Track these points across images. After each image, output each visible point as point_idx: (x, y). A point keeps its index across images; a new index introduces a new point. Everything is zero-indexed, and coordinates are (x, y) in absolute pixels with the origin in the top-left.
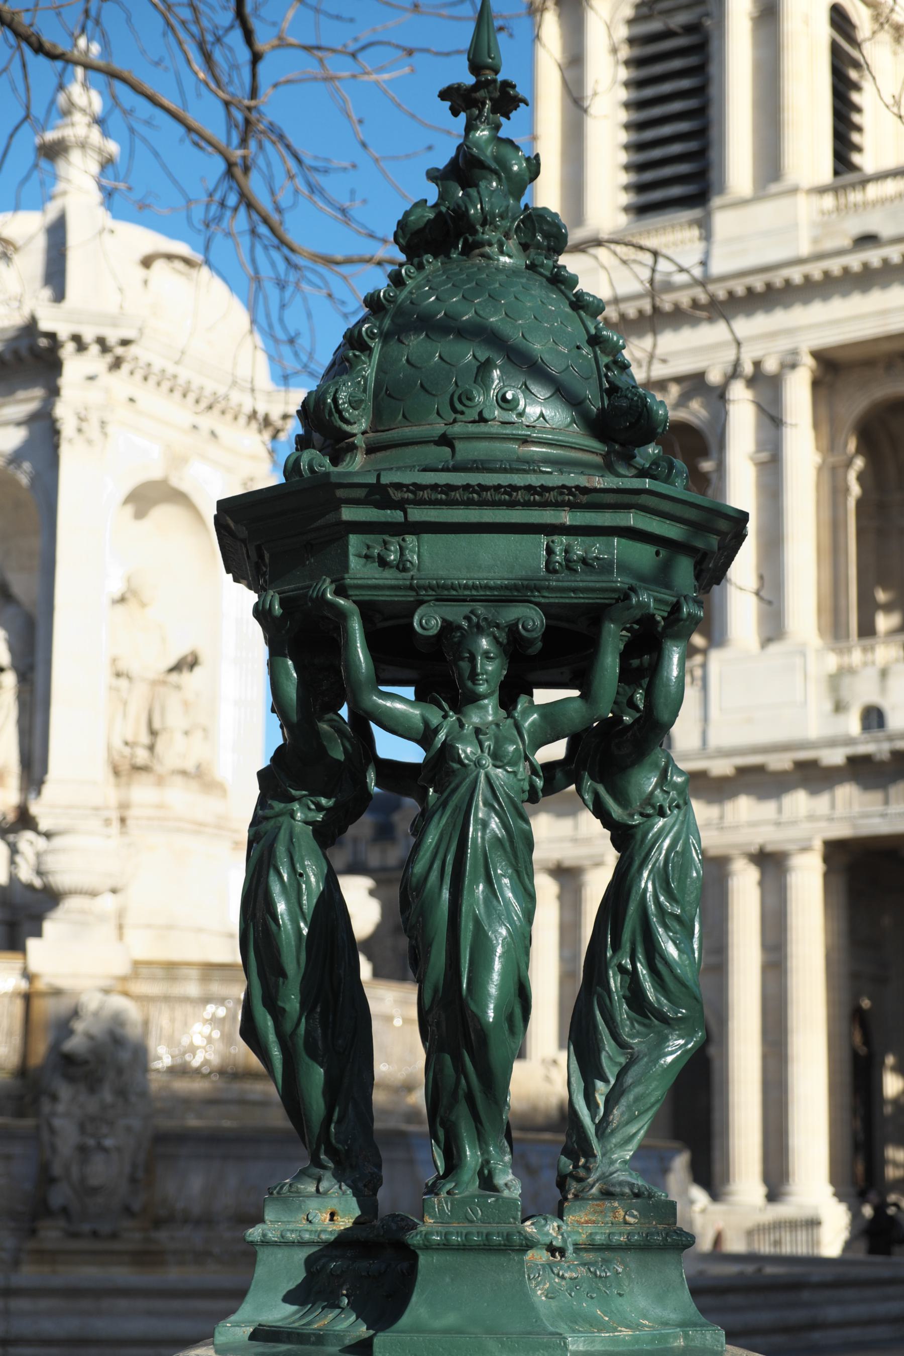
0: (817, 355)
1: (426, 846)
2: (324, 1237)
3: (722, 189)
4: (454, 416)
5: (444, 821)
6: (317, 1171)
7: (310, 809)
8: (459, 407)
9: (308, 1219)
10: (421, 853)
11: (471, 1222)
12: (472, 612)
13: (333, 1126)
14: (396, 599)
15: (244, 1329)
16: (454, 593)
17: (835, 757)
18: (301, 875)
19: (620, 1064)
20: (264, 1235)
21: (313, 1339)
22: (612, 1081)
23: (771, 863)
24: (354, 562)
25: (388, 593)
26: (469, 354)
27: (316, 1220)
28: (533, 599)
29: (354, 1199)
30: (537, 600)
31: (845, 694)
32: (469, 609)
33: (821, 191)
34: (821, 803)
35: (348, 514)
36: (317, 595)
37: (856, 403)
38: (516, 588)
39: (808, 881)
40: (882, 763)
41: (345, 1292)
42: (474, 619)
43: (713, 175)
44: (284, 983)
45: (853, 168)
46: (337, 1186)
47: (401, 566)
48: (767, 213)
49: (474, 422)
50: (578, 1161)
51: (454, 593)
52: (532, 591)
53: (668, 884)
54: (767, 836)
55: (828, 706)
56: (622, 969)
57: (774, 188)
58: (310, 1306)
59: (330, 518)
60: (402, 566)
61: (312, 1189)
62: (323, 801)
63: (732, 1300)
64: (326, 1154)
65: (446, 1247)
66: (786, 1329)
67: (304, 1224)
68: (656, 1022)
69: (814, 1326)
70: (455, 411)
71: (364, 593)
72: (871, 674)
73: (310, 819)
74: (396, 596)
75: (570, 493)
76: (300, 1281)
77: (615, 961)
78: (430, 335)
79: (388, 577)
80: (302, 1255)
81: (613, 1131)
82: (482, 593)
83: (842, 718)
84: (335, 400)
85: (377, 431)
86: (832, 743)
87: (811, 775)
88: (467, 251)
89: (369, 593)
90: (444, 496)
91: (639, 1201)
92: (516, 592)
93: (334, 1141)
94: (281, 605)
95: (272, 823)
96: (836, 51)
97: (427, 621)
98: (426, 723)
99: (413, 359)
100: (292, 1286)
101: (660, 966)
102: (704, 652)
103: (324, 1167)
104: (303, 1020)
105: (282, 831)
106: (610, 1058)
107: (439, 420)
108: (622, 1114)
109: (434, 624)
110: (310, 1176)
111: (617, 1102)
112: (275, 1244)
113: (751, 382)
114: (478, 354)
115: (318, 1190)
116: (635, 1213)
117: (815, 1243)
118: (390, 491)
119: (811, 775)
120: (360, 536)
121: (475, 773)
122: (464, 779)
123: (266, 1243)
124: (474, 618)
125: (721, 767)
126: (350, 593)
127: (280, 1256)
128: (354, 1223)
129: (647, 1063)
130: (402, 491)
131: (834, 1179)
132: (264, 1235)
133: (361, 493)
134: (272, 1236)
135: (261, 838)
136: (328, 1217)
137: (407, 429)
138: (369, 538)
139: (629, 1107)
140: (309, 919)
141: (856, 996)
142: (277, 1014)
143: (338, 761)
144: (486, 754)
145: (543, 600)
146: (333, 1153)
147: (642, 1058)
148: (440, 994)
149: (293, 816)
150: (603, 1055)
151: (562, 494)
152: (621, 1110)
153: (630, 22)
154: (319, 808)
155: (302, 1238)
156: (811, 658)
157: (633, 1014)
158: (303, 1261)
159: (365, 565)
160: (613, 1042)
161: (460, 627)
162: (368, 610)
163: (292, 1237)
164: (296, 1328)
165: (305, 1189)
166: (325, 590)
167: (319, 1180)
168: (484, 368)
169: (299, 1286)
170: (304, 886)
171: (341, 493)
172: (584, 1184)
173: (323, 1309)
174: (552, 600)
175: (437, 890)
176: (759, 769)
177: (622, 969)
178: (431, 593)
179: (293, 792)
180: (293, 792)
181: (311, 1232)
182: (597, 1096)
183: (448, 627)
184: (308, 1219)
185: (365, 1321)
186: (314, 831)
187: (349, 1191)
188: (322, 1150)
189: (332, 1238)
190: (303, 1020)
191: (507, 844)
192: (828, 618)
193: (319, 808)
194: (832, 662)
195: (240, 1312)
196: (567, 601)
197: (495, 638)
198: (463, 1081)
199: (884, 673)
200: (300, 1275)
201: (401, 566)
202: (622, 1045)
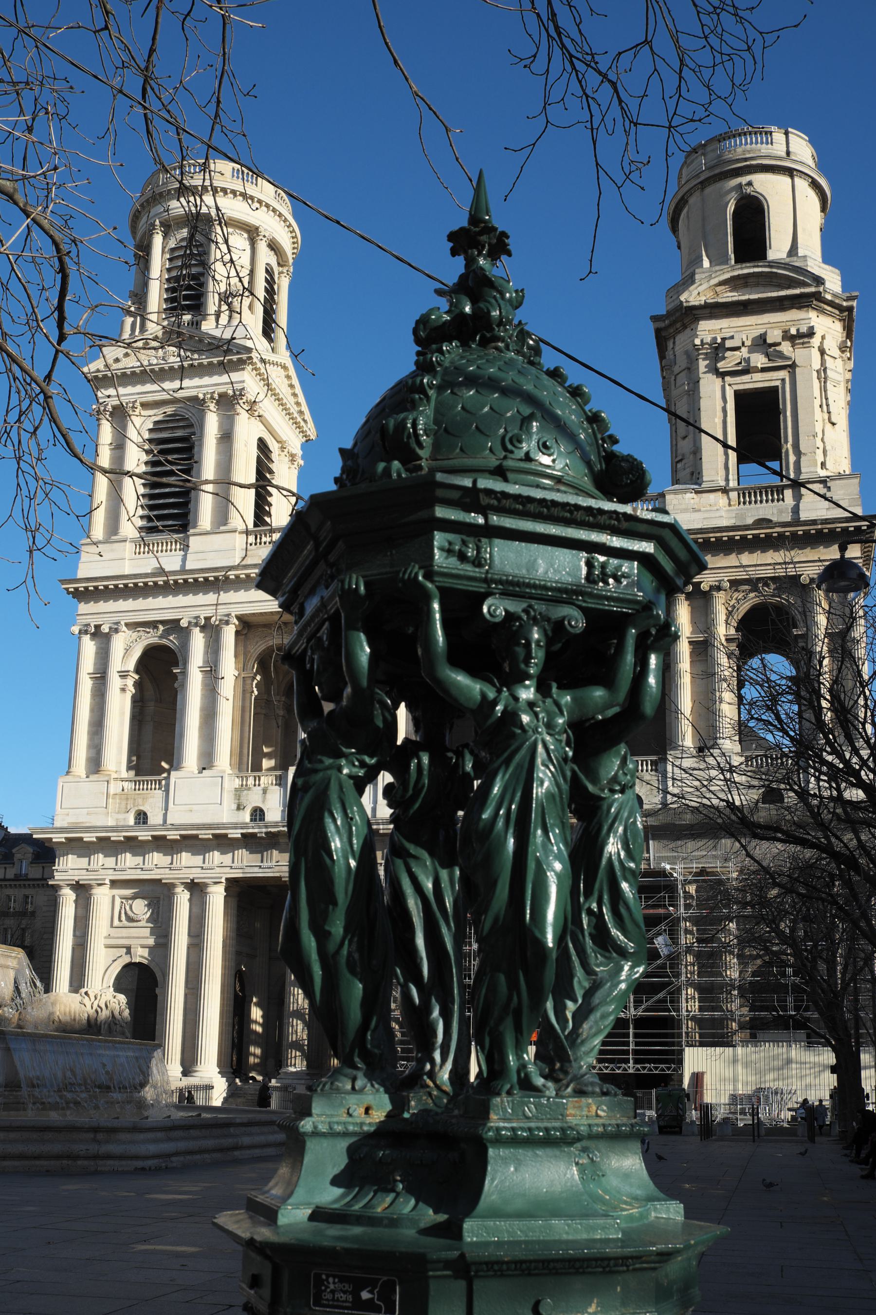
0: (238, 618)
1: (491, 798)
2: (366, 1128)
3: (195, 526)
4: (504, 453)
5: (507, 776)
6: (349, 1071)
7: (354, 765)
8: (510, 447)
9: (348, 1113)
10: (489, 802)
11: (528, 1118)
12: (530, 606)
13: (369, 1033)
14: (471, 589)
15: (304, 1211)
16: (517, 589)
17: (236, 834)
18: (352, 819)
19: (585, 988)
20: (315, 1127)
21: (385, 1222)
22: (580, 1001)
23: (197, 889)
24: (437, 553)
25: (465, 583)
26: (513, 409)
27: (355, 1114)
28: (577, 602)
29: (387, 1096)
30: (580, 603)
31: (243, 801)
32: (524, 605)
33: (247, 533)
34: (227, 859)
35: (441, 512)
36: (406, 576)
37: (258, 647)
38: (565, 591)
39: (217, 898)
40: (261, 838)
41: (398, 1178)
42: (532, 613)
43: (191, 517)
44: (333, 909)
45: (266, 524)
46: (369, 1085)
47: (476, 562)
48: (218, 540)
49: (521, 460)
50: (555, 1065)
51: (517, 589)
52: (577, 596)
53: (628, 845)
54: (196, 874)
55: (234, 806)
56: (590, 912)
57: (222, 528)
58: (357, 1189)
59: (423, 514)
60: (477, 562)
61: (349, 1087)
62: (367, 759)
63: (192, 1132)
64: (359, 1057)
65: (514, 1141)
66: (221, 1150)
67: (344, 1118)
68: (614, 955)
69: (236, 1148)
70: (505, 449)
71: (446, 580)
72: (258, 790)
73: (353, 774)
74: (472, 586)
75: (618, 519)
76: (342, 1167)
77: (586, 906)
78: (480, 390)
79: (468, 569)
80: (343, 1144)
81: (583, 1042)
82: (539, 592)
83: (241, 812)
84: (414, 425)
85: (437, 460)
86: (235, 826)
87: (222, 842)
88: (484, 343)
89: (450, 581)
90: (521, 507)
91: (608, 1098)
92: (565, 594)
93: (369, 1046)
94: (366, 585)
95: (321, 774)
96: (259, 461)
97: (494, 608)
98: (484, 696)
99: (468, 407)
100: (336, 1171)
101: (623, 911)
102: (169, 772)
103: (357, 1068)
104: (347, 942)
105: (332, 781)
106: (580, 982)
107: (491, 455)
108: (591, 1028)
109: (501, 612)
110: (346, 1076)
111: (586, 1018)
112: (323, 1135)
113: (203, 628)
114: (521, 410)
115: (353, 1088)
116: (605, 1108)
117: (208, 1098)
118: (481, 496)
119: (222, 842)
120: (443, 534)
121: (533, 738)
122: (524, 743)
123: (316, 1134)
124: (531, 611)
125: (173, 835)
126: (437, 579)
127: (325, 1145)
128: (386, 1116)
129: (610, 987)
130: (490, 497)
131: (219, 1065)
132: (315, 1127)
133: (455, 495)
134: (323, 1128)
135: (310, 788)
136: (363, 1110)
137: (466, 460)
138: (451, 537)
139: (596, 1022)
140: (357, 856)
141: (238, 964)
142: (322, 936)
143: (378, 727)
144: (541, 723)
145: (584, 605)
146: (366, 1056)
147: (606, 984)
148: (500, 923)
149: (340, 769)
150: (576, 980)
151: (611, 518)
152: (589, 1024)
153: (151, 431)
154: (363, 765)
155: (347, 1129)
156: (226, 779)
157: (596, 948)
158: (345, 1150)
159: (447, 558)
160: (582, 971)
161: (519, 618)
162: (447, 596)
163: (339, 1128)
164: (336, 1209)
165: (344, 1086)
166: (416, 575)
167: (354, 1080)
168: (525, 422)
169: (343, 1171)
170: (354, 828)
171: (440, 493)
172: (560, 1084)
173: (375, 1193)
174: (590, 605)
175: (503, 834)
176: (196, 837)
177: (590, 912)
178: (500, 587)
179: (344, 749)
180: (344, 749)
181: (354, 1124)
182: (567, 1013)
183: (510, 616)
184: (348, 1113)
185: (428, 1203)
186: (355, 784)
187: (382, 1089)
188: (356, 1054)
189: (372, 1129)
190: (347, 942)
191: (558, 799)
192: (236, 759)
193: (363, 765)
194: (237, 782)
195: (295, 1195)
196: (601, 607)
197: (545, 631)
198: (515, 998)
199: (265, 791)
200: (342, 1162)
201: (476, 562)
202: (588, 971)
